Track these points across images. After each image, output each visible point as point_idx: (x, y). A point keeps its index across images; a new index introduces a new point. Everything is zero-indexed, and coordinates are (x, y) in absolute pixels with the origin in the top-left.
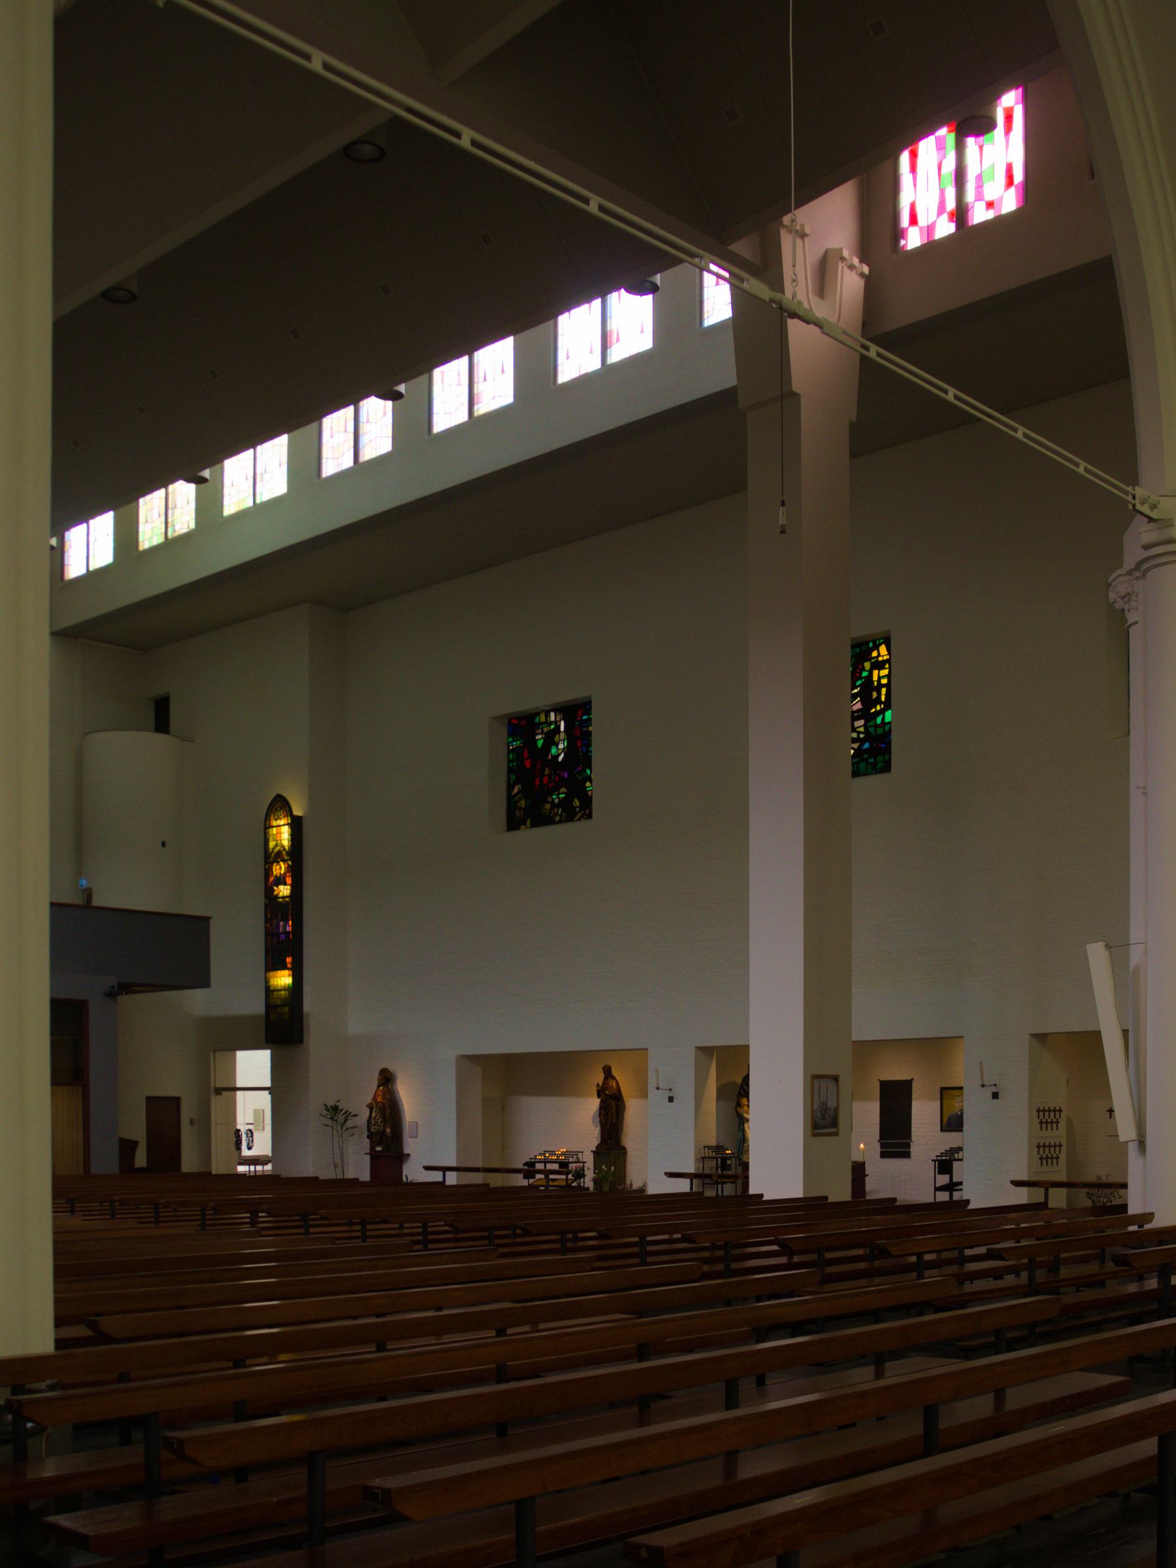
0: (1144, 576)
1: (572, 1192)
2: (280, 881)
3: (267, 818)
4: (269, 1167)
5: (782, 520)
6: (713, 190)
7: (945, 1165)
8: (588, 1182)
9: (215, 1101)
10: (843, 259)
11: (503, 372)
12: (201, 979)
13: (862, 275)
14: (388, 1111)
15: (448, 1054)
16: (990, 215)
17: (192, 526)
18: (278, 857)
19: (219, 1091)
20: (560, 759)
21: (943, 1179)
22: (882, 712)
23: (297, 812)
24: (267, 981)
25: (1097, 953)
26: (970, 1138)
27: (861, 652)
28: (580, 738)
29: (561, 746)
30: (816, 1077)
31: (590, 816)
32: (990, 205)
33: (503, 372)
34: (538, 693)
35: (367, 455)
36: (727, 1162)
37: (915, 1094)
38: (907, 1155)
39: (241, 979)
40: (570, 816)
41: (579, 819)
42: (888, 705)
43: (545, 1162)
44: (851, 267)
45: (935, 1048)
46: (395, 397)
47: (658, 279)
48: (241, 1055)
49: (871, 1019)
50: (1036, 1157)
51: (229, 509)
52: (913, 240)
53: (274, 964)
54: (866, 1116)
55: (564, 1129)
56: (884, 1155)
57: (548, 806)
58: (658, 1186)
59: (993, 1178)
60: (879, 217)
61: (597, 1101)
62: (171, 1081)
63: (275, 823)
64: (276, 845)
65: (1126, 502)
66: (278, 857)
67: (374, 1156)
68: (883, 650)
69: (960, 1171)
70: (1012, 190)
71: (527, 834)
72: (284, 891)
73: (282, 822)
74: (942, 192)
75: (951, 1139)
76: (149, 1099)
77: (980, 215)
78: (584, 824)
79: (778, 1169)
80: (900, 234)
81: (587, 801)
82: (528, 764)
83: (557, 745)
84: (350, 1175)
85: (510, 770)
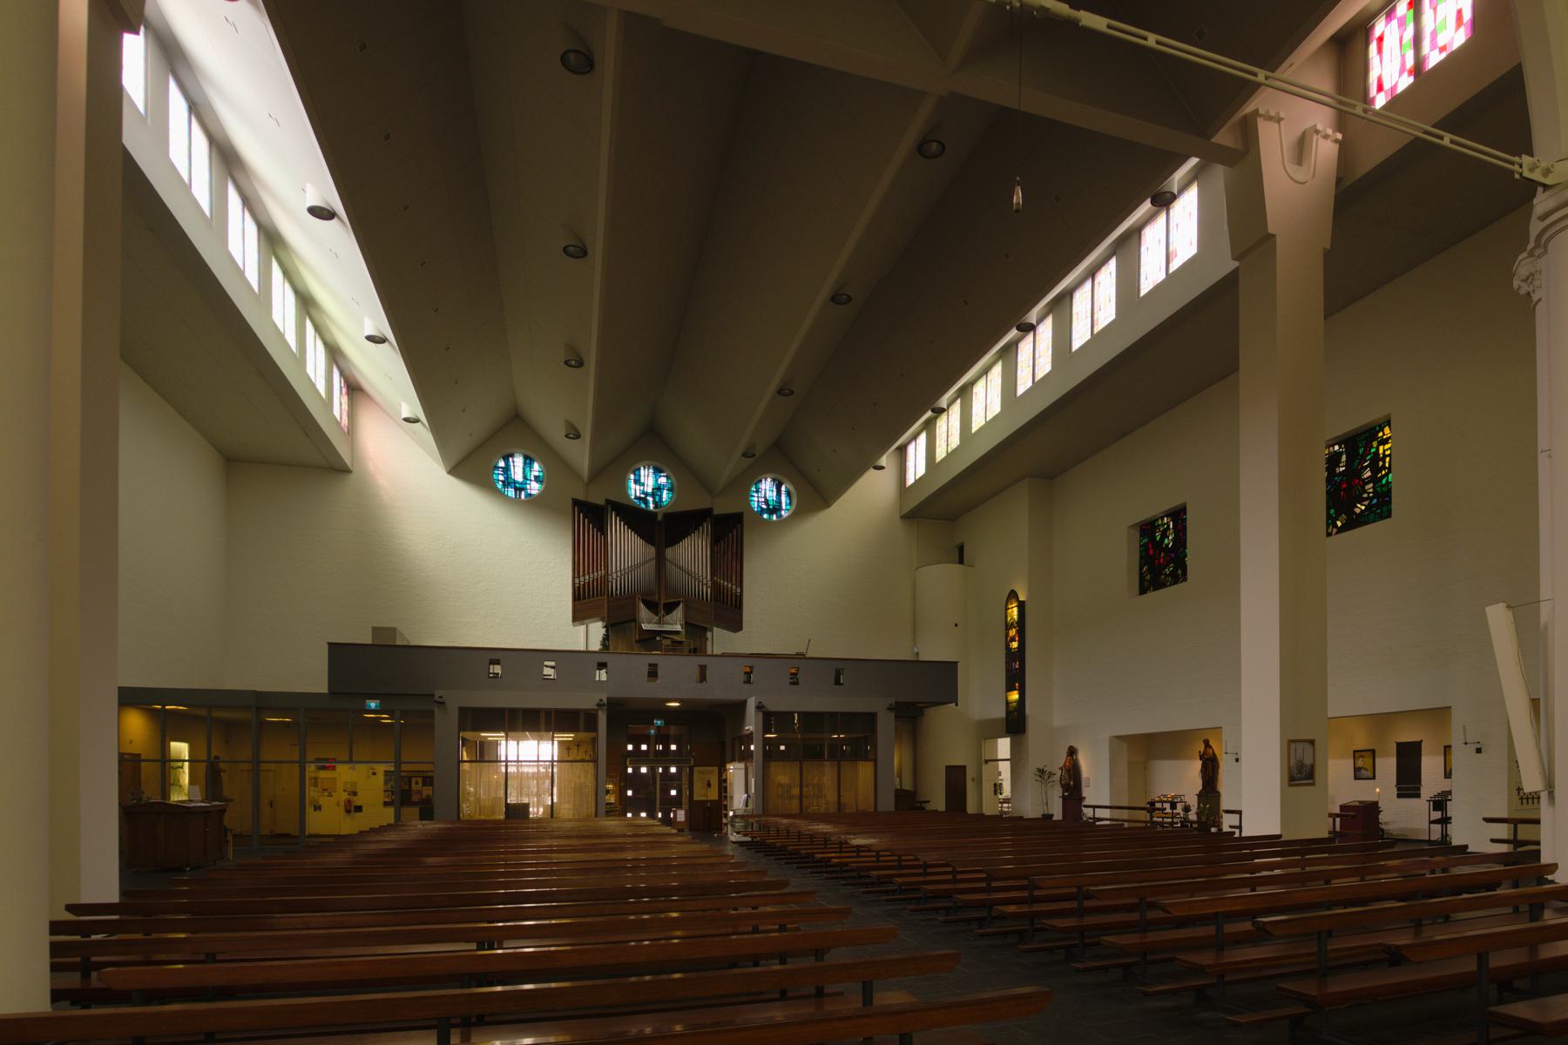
0: (1545, 247)
2: (1013, 639)
7: (1440, 803)
8: (1193, 816)
9: (985, 767)
10: (1317, 132)
13: (1336, 141)
16: (1444, 55)
21: (1437, 815)
25: (1498, 618)
26: (1457, 785)
28: (1181, 530)
30: (1290, 741)
32: (1442, 49)
34: (1154, 506)
39: (983, 695)
40: (1176, 582)
44: (1326, 137)
45: (1439, 716)
53: (1010, 688)
54: (1387, 766)
55: (1180, 781)
62: (959, 756)
65: (1512, 172)
67: (1064, 798)
69: (1453, 809)
70: (1462, 29)
71: (1153, 596)
72: (1015, 645)
74: (1403, 57)
76: (948, 768)
85: (1141, 557)
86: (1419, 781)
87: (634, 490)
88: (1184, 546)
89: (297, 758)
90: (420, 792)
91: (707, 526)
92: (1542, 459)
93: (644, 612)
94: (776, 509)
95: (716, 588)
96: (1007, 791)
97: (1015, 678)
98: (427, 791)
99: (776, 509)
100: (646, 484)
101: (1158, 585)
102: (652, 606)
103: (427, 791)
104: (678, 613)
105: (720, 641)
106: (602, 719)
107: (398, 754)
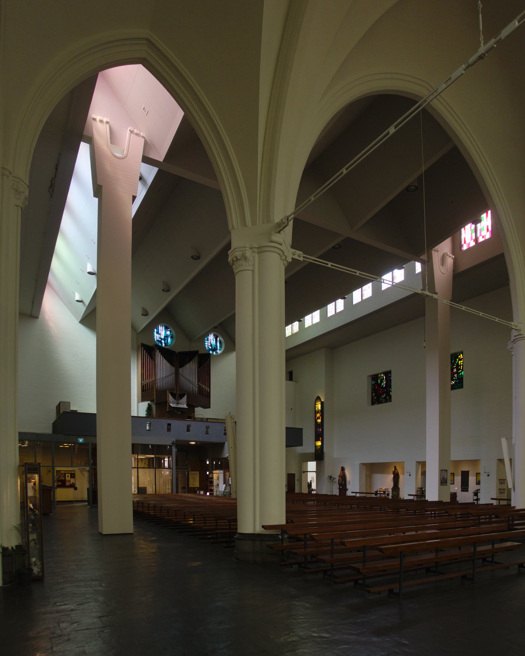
1: (386, 499)
3: (315, 402)
4: (315, 492)
5: (424, 345)
6: (414, 246)
7: (476, 494)
8: (390, 497)
9: (303, 474)
12: (301, 444)
14: (343, 477)
15: (358, 463)
16: (483, 239)
19: (304, 472)
21: (475, 498)
22: (461, 372)
23: (322, 400)
24: (315, 444)
25: (504, 441)
26: (482, 487)
27: (454, 357)
28: (389, 380)
30: (441, 470)
31: (391, 401)
32: (483, 237)
34: (379, 369)
35: (338, 311)
36: (421, 492)
37: (470, 475)
38: (468, 491)
39: (310, 444)
40: (386, 401)
42: (462, 370)
43: (380, 491)
44: (450, 257)
45: (475, 462)
46: (344, 298)
47: (404, 266)
48: (309, 463)
49: (456, 455)
50: (498, 492)
51: (306, 326)
52: (465, 247)
53: (317, 440)
54: (458, 479)
55: (384, 483)
56: (462, 491)
58: (407, 497)
59: (488, 496)
60: (457, 244)
61: (393, 475)
67: (340, 489)
68: (461, 355)
69: (480, 495)
71: (377, 406)
72: (319, 421)
75: (478, 487)
77: (481, 240)
78: (390, 403)
79: (432, 495)
80: (461, 246)
81: (390, 397)
82: (376, 388)
84: (334, 494)
85: (372, 389)
86: (468, 485)
87: (156, 337)
88: (390, 387)
89: (51, 465)
90: (69, 481)
91: (196, 359)
92: (514, 398)
93: (170, 398)
94: (215, 349)
95: (200, 388)
96: (314, 486)
97: (319, 436)
98: (72, 481)
99: (215, 349)
100: (161, 333)
101: (380, 402)
102: (174, 395)
103: (72, 481)
104: (185, 399)
105: (200, 412)
106: (174, 450)
107: (53, 463)
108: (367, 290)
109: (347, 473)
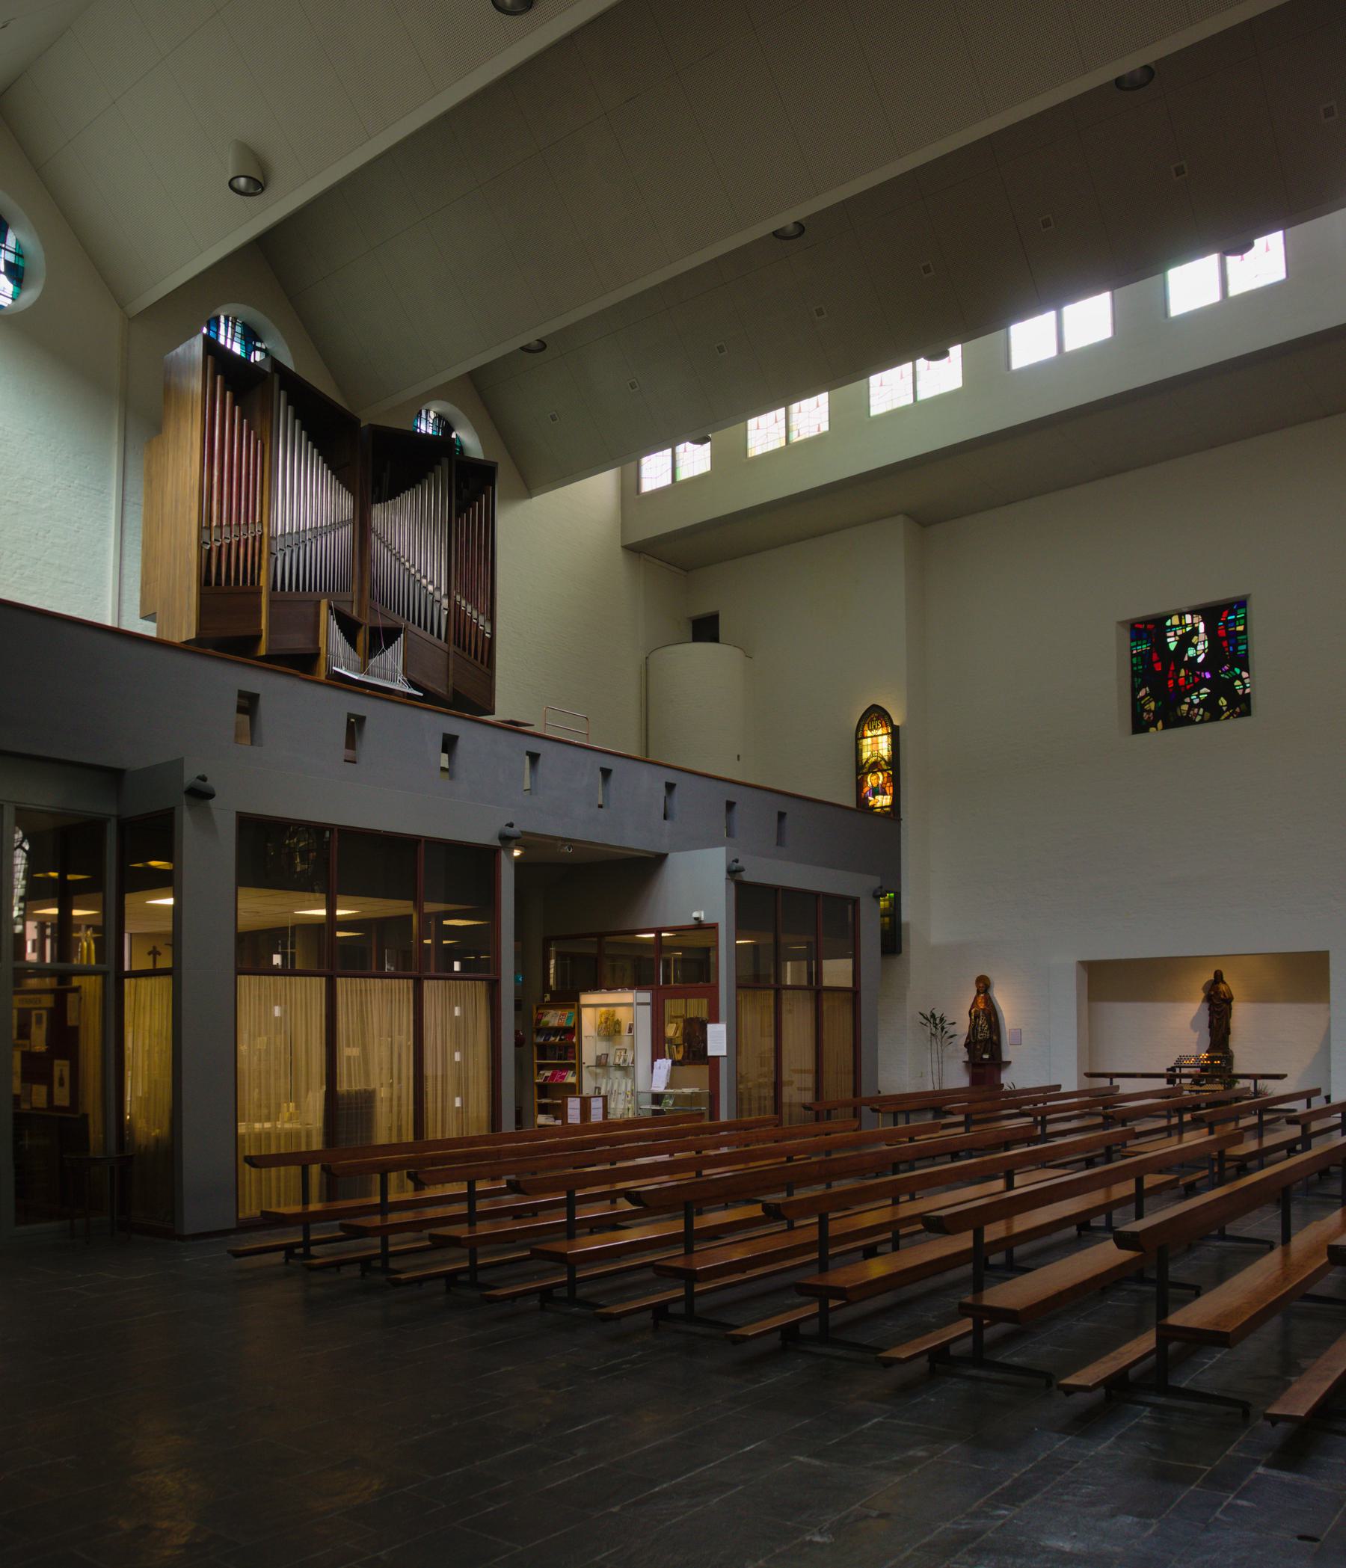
11: (1267, 250)
14: (986, 1018)
17: (709, 469)
18: (875, 767)
20: (1200, 660)
29: (1200, 647)
33: (1267, 250)
41: (1227, 718)
57: (1185, 707)
60: (631, 483)
63: (869, 733)
64: (872, 756)
66: (875, 767)
73: (880, 732)
83: (1195, 646)
85: (1134, 674)
95: (455, 610)
101: (1173, 720)
102: (349, 628)
108: (812, 415)
109: (1003, 1000)
